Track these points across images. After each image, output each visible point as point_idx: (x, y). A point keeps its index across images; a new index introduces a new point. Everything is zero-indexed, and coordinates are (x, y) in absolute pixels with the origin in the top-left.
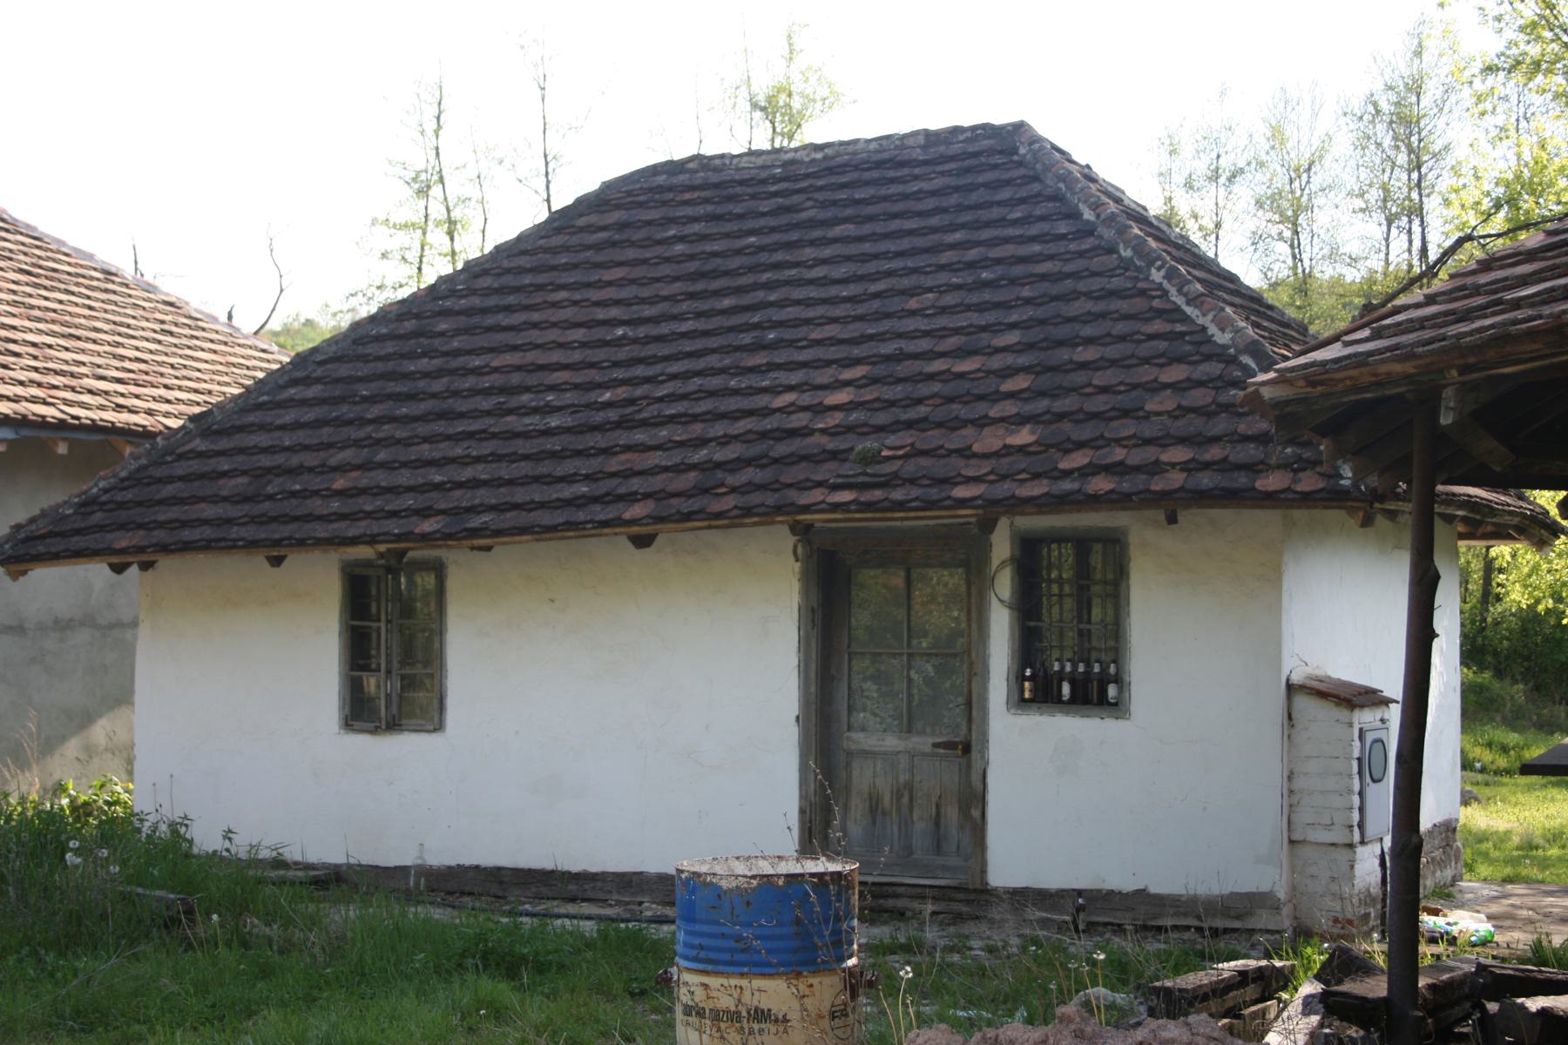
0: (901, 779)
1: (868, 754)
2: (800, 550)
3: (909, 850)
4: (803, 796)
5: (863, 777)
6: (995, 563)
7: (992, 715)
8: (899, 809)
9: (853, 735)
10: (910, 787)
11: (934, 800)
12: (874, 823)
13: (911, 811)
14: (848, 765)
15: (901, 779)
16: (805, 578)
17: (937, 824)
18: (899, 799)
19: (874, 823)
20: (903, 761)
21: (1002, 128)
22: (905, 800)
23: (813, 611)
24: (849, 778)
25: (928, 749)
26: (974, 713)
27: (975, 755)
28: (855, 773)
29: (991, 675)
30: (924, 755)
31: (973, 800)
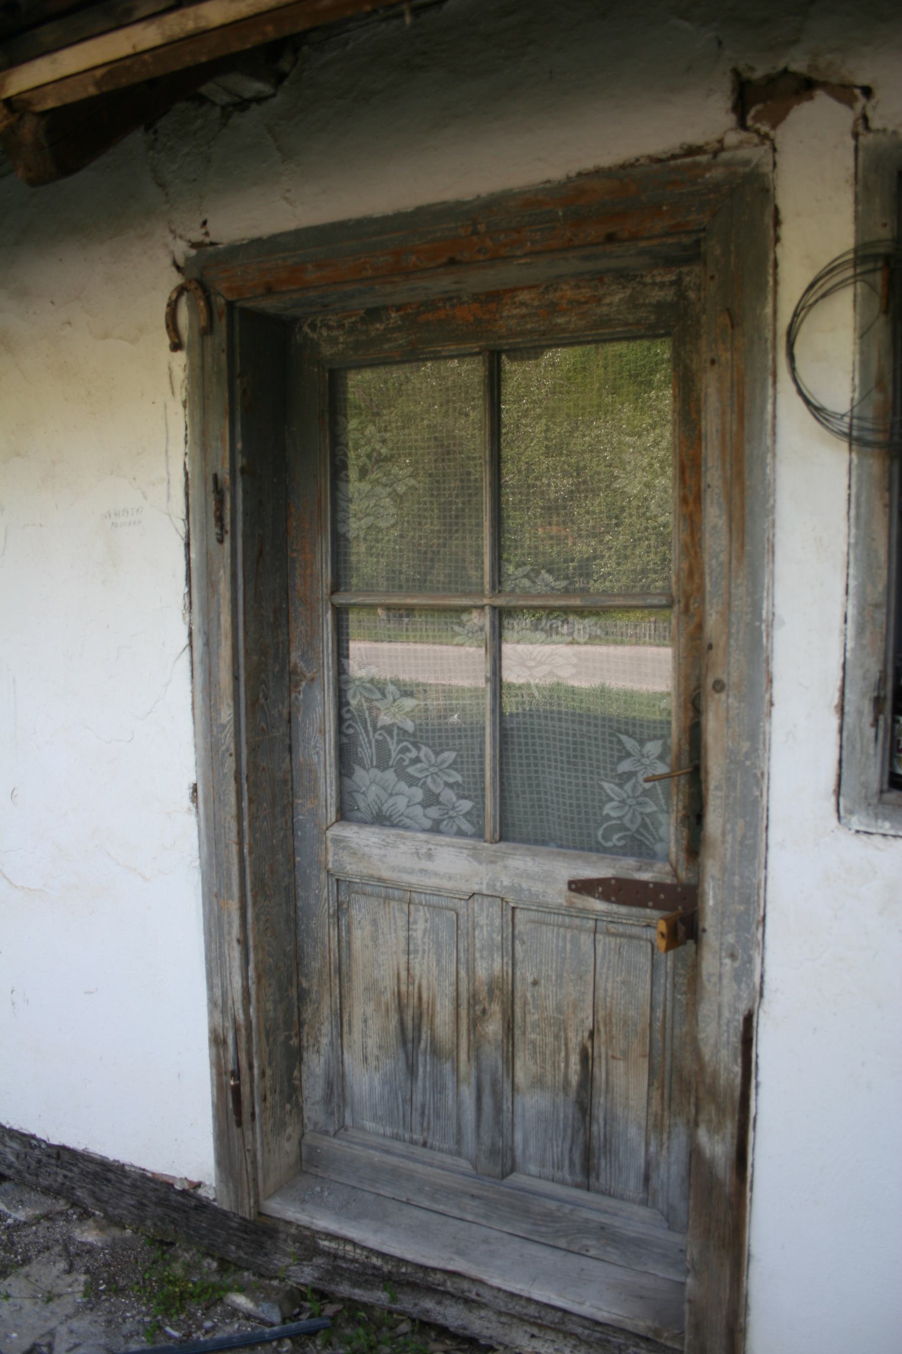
0: (482, 973)
1: (390, 892)
2: (183, 317)
3: (503, 1161)
4: (218, 1003)
5: (380, 953)
6: (794, 273)
7: (778, 834)
8: (476, 1050)
9: (351, 833)
10: (505, 992)
11: (576, 1039)
12: (411, 1070)
13: (510, 1061)
14: (340, 911)
15: (482, 973)
16: (199, 400)
17: (584, 1108)
18: (475, 1023)
19: (411, 1070)
20: (487, 921)
21: (610, 168)
22: (493, 1027)
23: (219, 492)
24: (344, 946)
25: (557, 893)
26: (714, 821)
27: (713, 962)
28: (360, 936)
29: (781, 690)
30: (544, 908)
31: (710, 1096)
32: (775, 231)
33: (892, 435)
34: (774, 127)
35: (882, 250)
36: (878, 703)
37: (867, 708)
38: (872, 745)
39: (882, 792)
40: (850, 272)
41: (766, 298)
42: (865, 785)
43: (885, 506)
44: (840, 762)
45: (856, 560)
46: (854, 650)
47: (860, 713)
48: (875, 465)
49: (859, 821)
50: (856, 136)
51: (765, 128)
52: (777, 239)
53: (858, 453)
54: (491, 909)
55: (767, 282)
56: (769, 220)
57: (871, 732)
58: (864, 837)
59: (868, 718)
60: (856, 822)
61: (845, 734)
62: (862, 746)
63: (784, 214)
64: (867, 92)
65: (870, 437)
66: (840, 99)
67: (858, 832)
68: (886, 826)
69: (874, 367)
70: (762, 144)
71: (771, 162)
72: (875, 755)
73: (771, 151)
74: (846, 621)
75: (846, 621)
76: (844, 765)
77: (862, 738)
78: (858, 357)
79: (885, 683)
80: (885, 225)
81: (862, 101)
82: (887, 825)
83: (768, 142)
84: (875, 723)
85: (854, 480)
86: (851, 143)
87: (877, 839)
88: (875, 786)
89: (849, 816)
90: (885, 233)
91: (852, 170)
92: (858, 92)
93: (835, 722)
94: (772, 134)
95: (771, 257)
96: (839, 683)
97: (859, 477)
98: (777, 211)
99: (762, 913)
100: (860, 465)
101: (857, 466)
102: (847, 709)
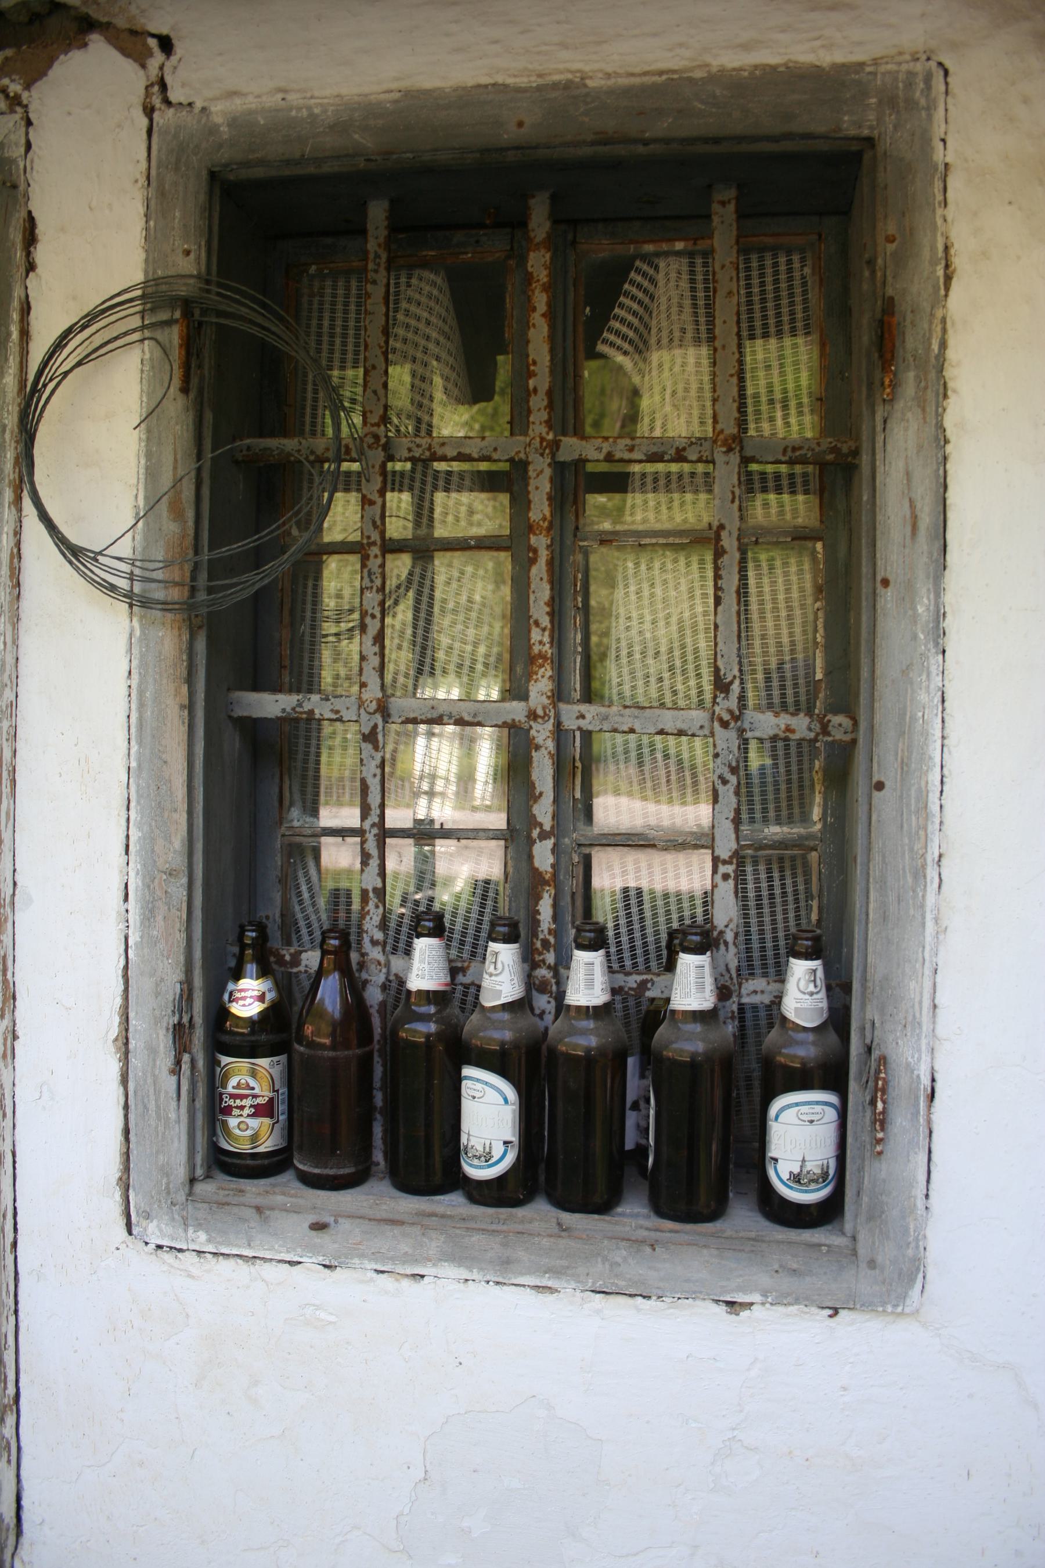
32: (28, 254)
33: (193, 590)
34: (28, 87)
35: (182, 291)
36: (180, 1033)
37: (164, 1042)
38: (173, 1104)
39: (192, 1181)
40: (136, 322)
41: (7, 360)
42: (165, 1171)
43: (182, 707)
44: (126, 1132)
45: (139, 796)
46: (139, 945)
47: (152, 1050)
48: (168, 640)
49: (161, 1231)
50: (149, 111)
51: (15, 88)
52: (31, 267)
53: (141, 618)
54: (661, 838)
55: (9, 334)
56: (16, 236)
57: (169, 1083)
58: (168, 1257)
59: (165, 1060)
60: (155, 1231)
61: (131, 1086)
62: (158, 1107)
63: (42, 229)
64: (166, 44)
65: (159, 593)
66: (125, 53)
67: (159, 1247)
68: (201, 1239)
69: (166, 480)
70: (12, 111)
71: (23, 141)
72: (178, 1121)
73: (23, 123)
74: (126, 899)
75: (126, 899)
76: (132, 1136)
77: (157, 1092)
78: (143, 461)
79: (190, 999)
80: (187, 253)
81: (159, 57)
82: (202, 1236)
83: (19, 109)
84: (176, 1069)
85: (135, 663)
86: (144, 122)
87: (189, 1259)
88: (181, 1173)
89: (144, 1223)
90: (187, 266)
91: (144, 165)
92: (152, 42)
93: (114, 1067)
94: (25, 95)
95: (18, 292)
96: (119, 1001)
97: (142, 656)
98: (31, 221)
99: (11, 1390)
100: (144, 637)
101: (140, 640)
102: (132, 1044)
